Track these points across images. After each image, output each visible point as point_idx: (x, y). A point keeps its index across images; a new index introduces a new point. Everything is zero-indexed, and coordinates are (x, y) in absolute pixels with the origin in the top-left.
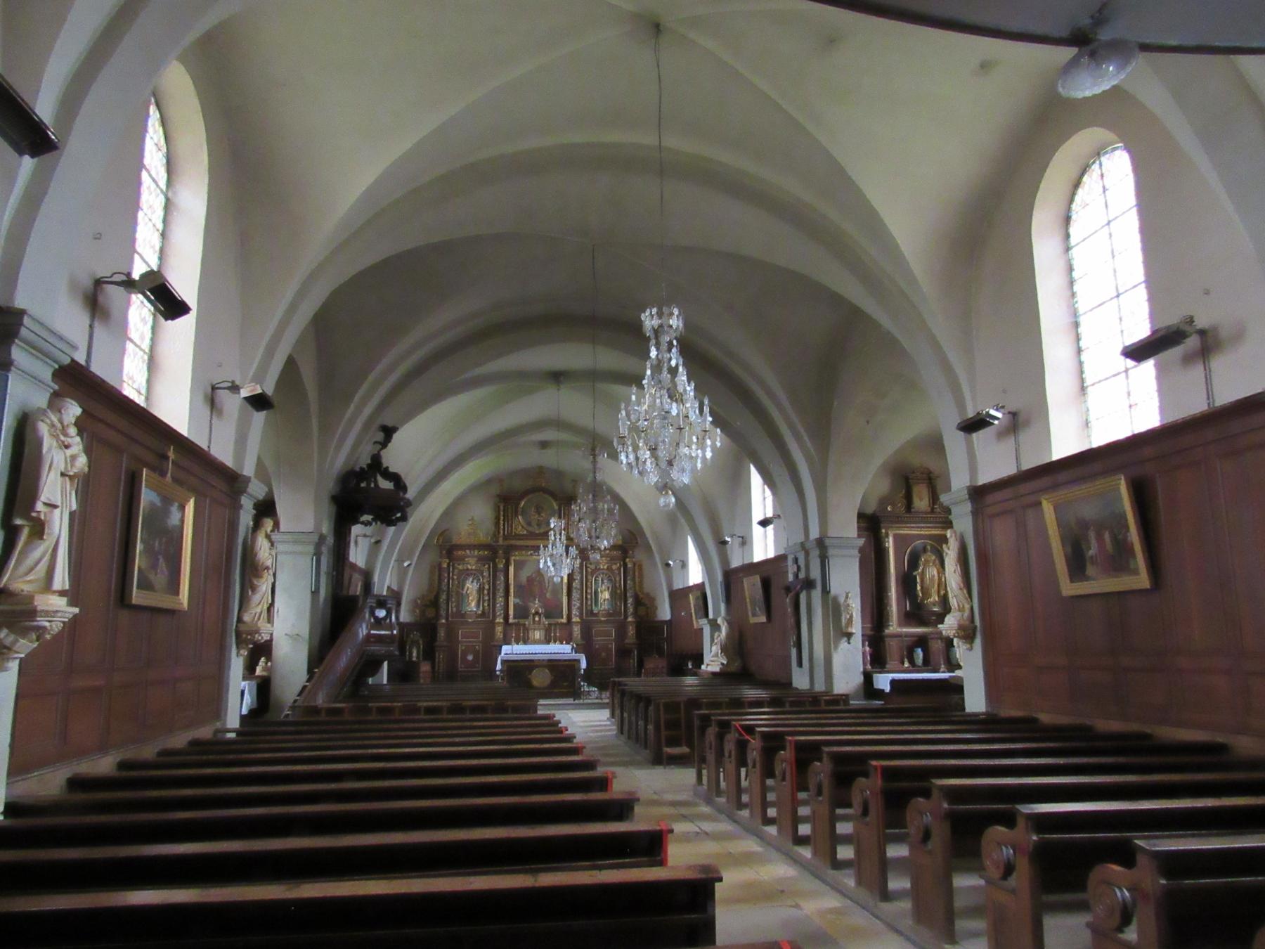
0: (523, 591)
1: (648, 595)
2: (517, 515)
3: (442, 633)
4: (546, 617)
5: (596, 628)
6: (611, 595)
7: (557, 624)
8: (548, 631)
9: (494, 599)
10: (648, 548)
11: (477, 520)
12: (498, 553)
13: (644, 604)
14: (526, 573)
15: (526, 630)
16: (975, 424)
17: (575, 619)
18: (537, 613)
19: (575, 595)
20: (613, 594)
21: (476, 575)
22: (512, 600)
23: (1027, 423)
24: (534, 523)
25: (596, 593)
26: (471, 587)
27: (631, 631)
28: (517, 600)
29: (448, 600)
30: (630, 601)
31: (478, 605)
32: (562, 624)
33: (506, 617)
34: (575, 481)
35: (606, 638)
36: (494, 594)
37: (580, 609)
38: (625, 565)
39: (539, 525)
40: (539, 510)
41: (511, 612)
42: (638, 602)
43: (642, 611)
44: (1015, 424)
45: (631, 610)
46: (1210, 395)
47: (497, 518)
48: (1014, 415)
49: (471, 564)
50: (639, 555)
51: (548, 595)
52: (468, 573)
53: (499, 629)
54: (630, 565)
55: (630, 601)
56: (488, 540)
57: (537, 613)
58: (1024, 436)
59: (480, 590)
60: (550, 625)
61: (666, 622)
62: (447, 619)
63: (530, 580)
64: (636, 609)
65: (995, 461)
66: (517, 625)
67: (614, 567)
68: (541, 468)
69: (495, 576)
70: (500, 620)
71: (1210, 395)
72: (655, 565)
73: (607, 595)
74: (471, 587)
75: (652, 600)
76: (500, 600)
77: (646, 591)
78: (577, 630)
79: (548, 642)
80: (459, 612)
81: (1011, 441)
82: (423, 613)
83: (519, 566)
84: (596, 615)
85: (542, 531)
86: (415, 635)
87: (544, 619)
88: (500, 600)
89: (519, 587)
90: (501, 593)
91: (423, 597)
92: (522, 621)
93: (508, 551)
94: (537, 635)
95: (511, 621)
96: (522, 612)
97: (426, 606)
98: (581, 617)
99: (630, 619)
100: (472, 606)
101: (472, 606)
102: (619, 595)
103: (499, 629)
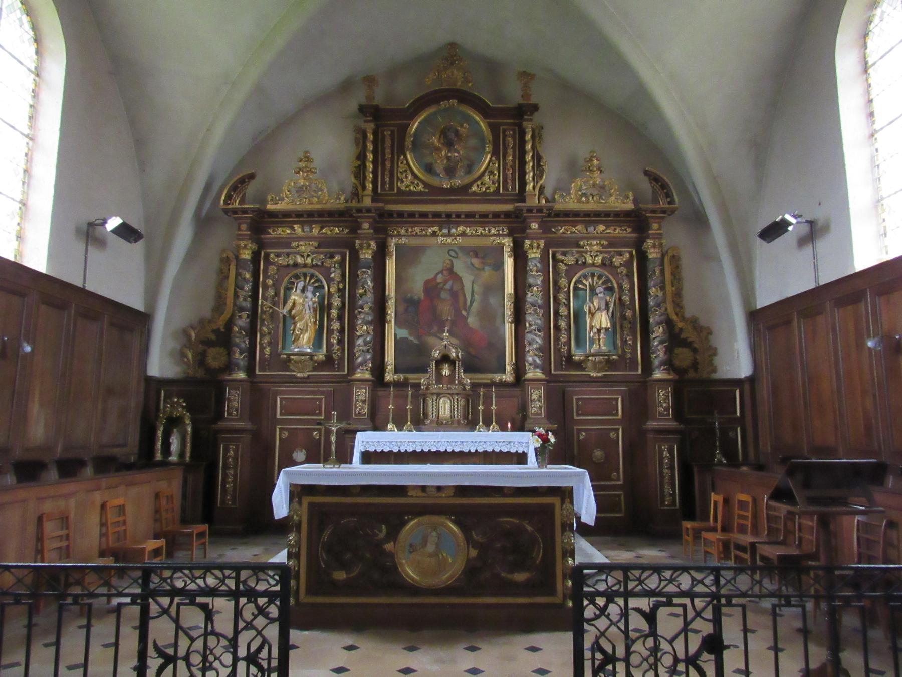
0: (420, 311)
1: (694, 323)
2: (402, 151)
3: (234, 400)
4: (468, 369)
5: (580, 395)
6: (612, 318)
7: (493, 384)
8: (470, 397)
9: (353, 328)
10: (698, 220)
11: (320, 163)
12: (365, 224)
13: (689, 342)
14: (420, 276)
15: (420, 395)
16: (774, 230)
17: (532, 373)
18: (445, 358)
19: (533, 319)
20: (618, 320)
21: (312, 275)
22: (391, 331)
23: (826, 229)
24: (440, 167)
25: (579, 316)
26: (302, 301)
27: (663, 399)
28: (404, 333)
29: (252, 332)
30: (658, 333)
31: (317, 342)
32: (502, 384)
33: (379, 368)
34: (526, 76)
35: (603, 413)
36: (353, 318)
37: (545, 350)
38: (642, 257)
39: (450, 171)
40: (449, 139)
41: (390, 357)
42: (674, 339)
43: (683, 356)
44: (813, 232)
45: (659, 354)
46: (817, 278)
47: (362, 157)
48: (811, 223)
49: (304, 252)
50: (670, 235)
51: (472, 321)
52: (295, 272)
53: (361, 394)
54: (653, 254)
55: (658, 333)
56: (337, 203)
57: (445, 358)
58: (822, 245)
59: (323, 309)
60: (475, 386)
61: (738, 382)
62: (250, 370)
63: (431, 288)
64: (669, 350)
65: (784, 276)
66: (400, 385)
67: (617, 261)
68: (453, 45)
69: (354, 281)
70: (364, 374)
71: (817, 278)
72: (711, 257)
73: (603, 320)
74: (302, 301)
75: (705, 332)
76: (364, 330)
77: (690, 311)
78: (536, 398)
79: (471, 425)
80: (275, 354)
81: (808, 249)
82: (201, 360)
83: (407, 257)
84: (579, 365)
85: (458, 182)
86: (178, 407)
87: (461, 373)
88: (364, 330)
89: (408, 304)
90: (366, 314)
91: (202, 323)
92: (413, 377)
93: (384, 222)
94: (445, 408)
95: (389, 377)
96: (414, 358)
97: (209, 343)
98: (546, 369)
99: (658, 375)
100: (304, 342)
101: (304, 342)
102: (634, 321)
103: (361, 394)
